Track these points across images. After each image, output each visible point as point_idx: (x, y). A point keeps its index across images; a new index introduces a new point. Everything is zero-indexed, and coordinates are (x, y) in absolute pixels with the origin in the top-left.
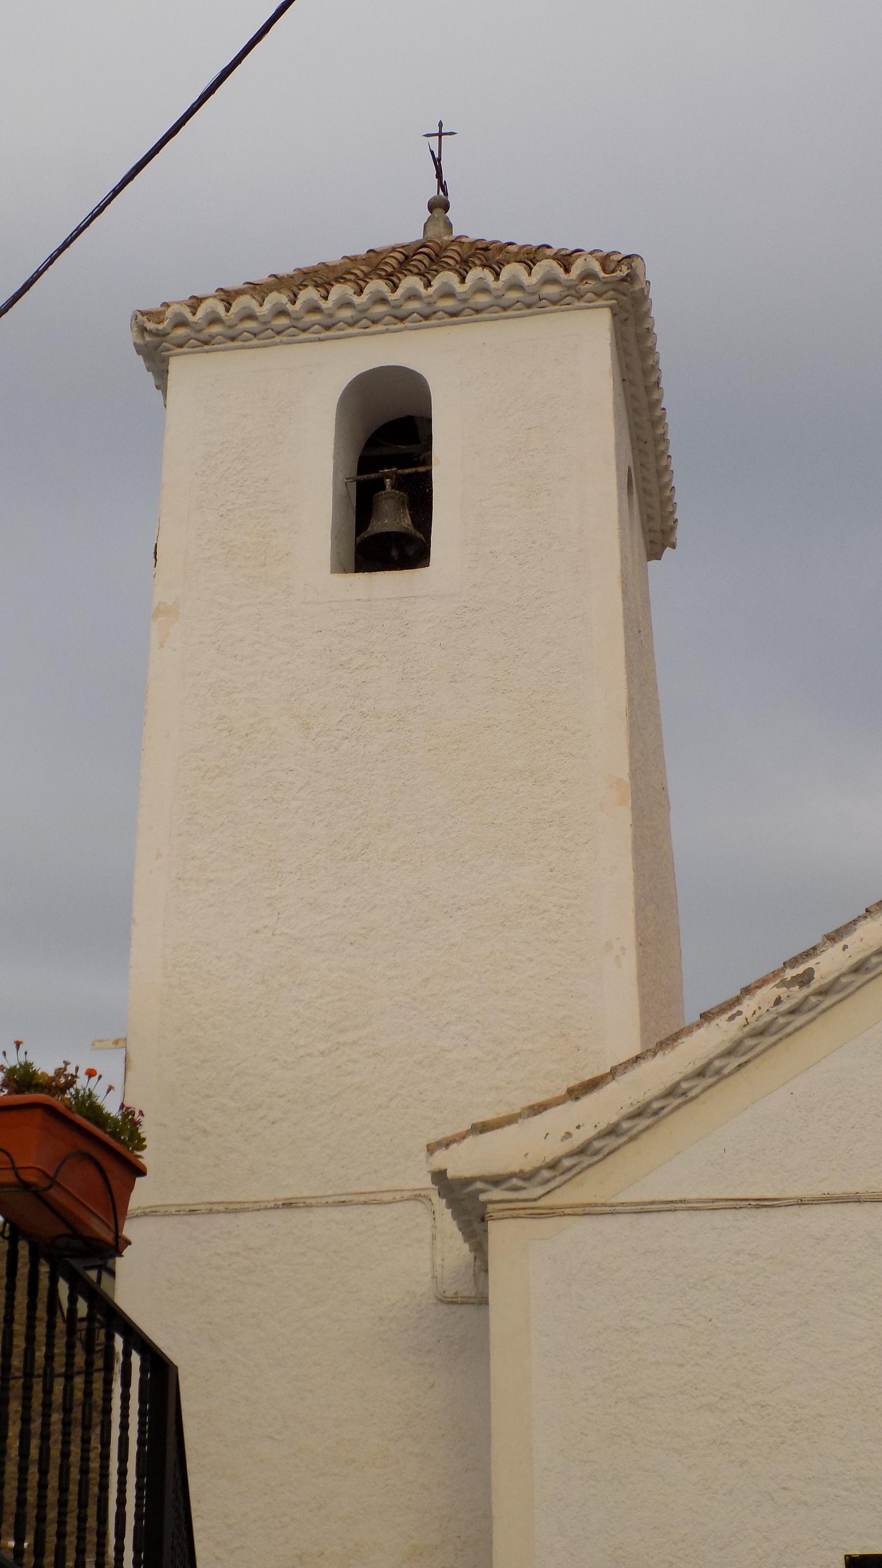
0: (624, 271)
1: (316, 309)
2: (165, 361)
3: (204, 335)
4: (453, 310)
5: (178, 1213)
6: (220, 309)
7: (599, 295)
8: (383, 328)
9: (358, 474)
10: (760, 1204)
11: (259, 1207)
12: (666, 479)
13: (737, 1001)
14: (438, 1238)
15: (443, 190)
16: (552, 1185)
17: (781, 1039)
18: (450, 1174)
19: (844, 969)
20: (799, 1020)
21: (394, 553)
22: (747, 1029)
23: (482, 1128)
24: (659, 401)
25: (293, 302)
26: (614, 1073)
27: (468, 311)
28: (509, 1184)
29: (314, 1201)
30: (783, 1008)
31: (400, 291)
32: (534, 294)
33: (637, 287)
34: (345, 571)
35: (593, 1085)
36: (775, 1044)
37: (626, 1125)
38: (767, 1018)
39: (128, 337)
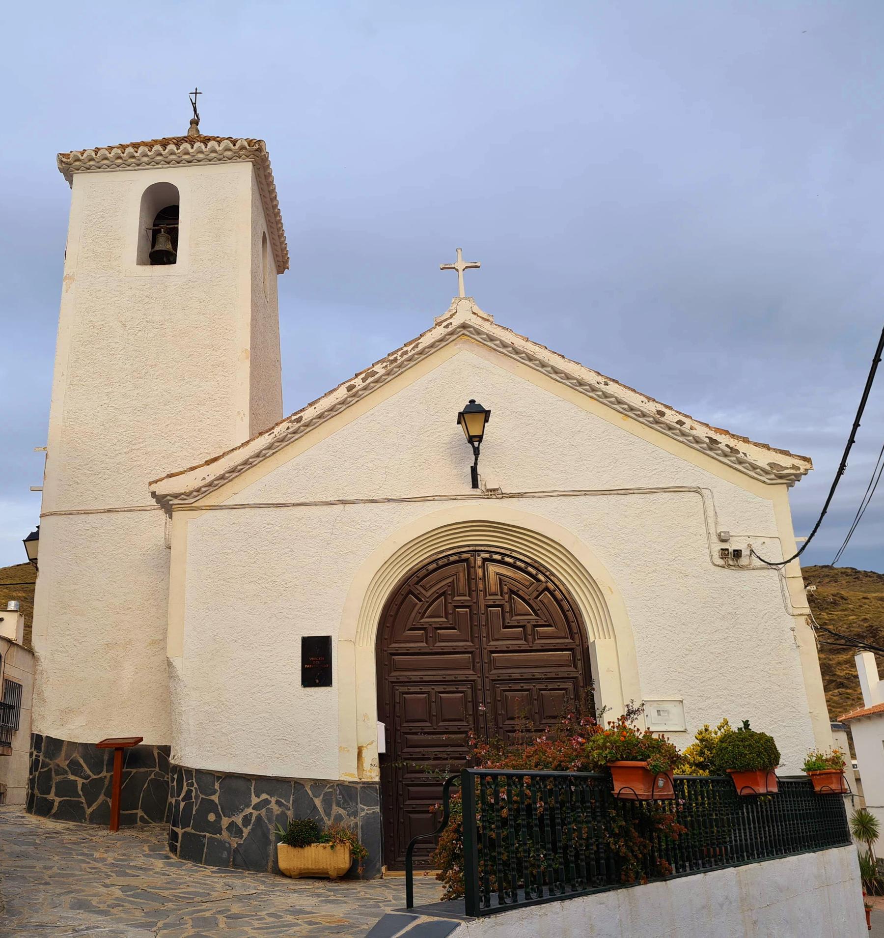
0: (257, 146)
1: (133, 157)
2: (72, 176)
3: (87, 165)
4: (189, 160)
5: (65, 514)
6: (93, 154)
7: (247, 157)
8: (161, 166)
13: (273, 428)
14: (168, 524)
15: (197, 116)
16: (198, 498)
18: (157, 493)
19: (314, 416)
21: (165, 259)
22: (275, 439)
23: (170, 476)
24: (277, 206)
25: (123, 153)
26: (223, 455)
27: (195, 161)
28: (180, 498)
29: (119, 510)
30: (290, 431)
31: (167, 150)
32: (221, 154)
33: (263, 154)
35: (215, 460)
36: (287, 445)
39: (55, 164)
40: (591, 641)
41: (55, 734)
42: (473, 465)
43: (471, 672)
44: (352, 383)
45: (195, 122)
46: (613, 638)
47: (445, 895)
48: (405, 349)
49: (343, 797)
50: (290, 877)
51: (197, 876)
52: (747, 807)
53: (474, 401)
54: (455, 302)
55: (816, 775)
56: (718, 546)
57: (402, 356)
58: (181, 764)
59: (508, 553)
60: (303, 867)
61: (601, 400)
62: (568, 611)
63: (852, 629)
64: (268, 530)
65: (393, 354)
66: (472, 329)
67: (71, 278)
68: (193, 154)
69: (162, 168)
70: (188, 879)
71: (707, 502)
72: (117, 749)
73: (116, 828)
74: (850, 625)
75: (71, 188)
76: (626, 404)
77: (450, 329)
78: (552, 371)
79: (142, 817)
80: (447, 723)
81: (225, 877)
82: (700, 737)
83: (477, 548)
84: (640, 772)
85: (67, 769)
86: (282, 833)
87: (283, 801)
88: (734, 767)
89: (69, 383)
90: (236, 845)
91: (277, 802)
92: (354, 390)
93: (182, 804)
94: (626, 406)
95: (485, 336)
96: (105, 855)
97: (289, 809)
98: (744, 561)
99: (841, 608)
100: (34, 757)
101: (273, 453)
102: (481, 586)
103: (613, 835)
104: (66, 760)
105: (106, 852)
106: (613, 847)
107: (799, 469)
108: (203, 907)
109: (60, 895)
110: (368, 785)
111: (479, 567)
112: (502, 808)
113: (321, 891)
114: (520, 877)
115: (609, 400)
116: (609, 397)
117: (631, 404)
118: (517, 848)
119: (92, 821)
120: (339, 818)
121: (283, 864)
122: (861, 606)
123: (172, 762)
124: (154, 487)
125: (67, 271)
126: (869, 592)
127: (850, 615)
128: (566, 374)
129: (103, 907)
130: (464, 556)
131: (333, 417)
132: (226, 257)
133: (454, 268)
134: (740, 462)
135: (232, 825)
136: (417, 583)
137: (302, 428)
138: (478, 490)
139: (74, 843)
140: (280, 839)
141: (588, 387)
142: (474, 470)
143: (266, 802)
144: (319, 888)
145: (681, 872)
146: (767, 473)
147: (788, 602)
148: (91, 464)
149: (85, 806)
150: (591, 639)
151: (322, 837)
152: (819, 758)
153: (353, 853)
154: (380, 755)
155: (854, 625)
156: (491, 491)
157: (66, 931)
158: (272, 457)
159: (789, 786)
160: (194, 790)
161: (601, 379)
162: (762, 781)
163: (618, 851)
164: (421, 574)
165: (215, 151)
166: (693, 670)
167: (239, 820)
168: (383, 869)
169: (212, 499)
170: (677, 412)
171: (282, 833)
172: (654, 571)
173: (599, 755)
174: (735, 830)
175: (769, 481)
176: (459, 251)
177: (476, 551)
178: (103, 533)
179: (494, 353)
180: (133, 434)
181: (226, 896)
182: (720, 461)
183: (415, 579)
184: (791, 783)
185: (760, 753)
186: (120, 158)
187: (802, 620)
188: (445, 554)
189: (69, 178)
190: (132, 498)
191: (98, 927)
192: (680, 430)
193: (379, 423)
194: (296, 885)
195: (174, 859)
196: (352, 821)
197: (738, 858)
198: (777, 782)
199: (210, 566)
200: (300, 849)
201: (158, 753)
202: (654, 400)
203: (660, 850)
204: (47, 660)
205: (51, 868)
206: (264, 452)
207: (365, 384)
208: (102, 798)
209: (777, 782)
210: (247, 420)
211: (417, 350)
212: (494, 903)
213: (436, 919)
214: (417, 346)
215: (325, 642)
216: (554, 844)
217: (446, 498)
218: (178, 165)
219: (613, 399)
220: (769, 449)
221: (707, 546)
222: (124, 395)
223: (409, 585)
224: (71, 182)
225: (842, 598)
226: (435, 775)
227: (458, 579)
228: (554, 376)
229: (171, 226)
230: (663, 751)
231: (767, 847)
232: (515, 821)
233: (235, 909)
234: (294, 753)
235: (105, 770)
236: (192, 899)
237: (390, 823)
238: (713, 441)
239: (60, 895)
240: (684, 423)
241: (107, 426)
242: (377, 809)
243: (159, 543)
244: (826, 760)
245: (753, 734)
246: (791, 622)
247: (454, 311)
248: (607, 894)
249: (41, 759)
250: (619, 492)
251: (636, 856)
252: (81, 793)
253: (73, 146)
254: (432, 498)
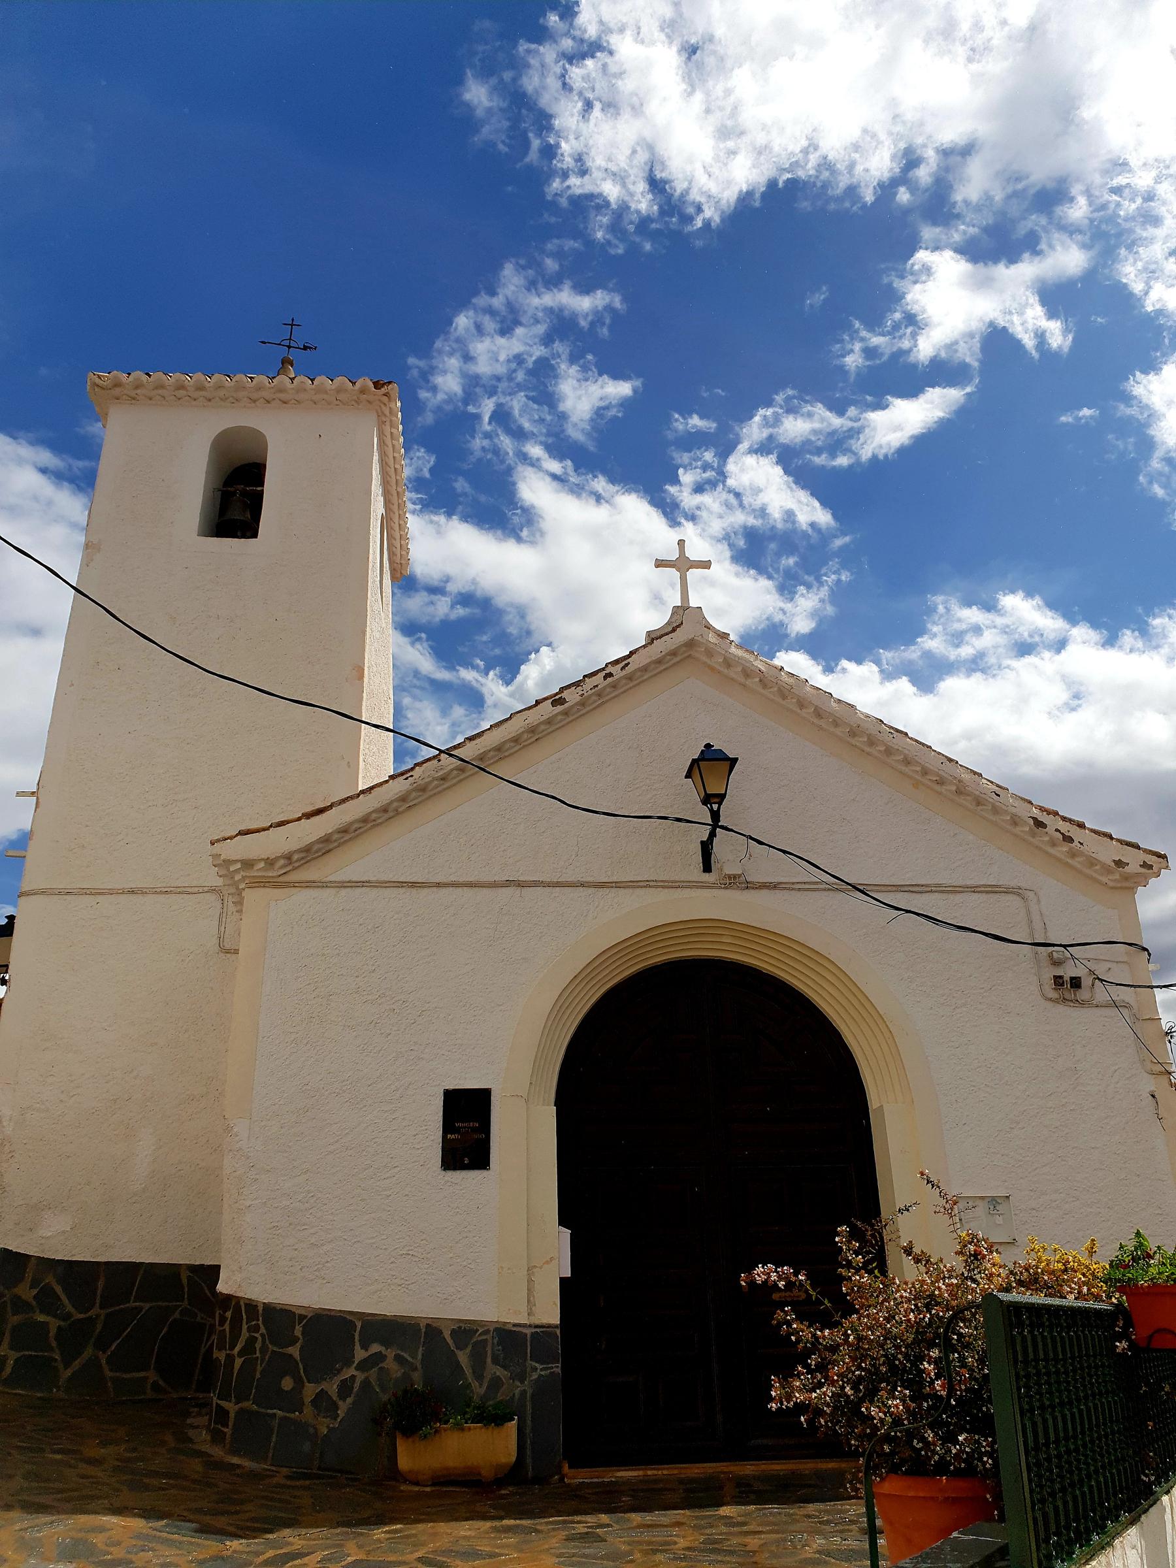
9: (223, 487)
10: (413, 885)
11: (111, 892)
17: (435, 794)
26: (331, 806)
85: (34, 1303)
87: (406, 1356)
91: (398, 1358)
93: (238, 1362)
143: (380, 1357)
160: (260, 1338)
215: (483, 1097)
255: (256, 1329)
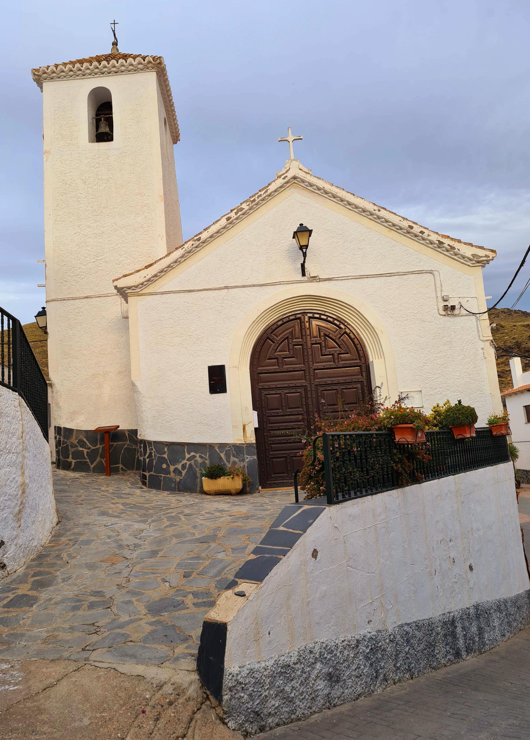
0: (158, 61)
1: (80, 70)
2: (42, 84)
4: (116, 71)
5: (61, 300)
6: (55, 69)
8: (98, 76)
12: (176, 122)
13: (184, 245)
18: (118, 287)
20: (198, 249)
23: (125, 276)
24: (172, 100)
25: (74, 68)
26: (155, 262)
27: (119, 72)
30: (194, 246)
31: (101, 65)
33: (162, 66)
34: (93, 142)
35: (151, 265)
36: (193, 255)
37: (158, 274)
38: (190, 249)
39: (31, 77)
40: (371, 361)
41: (68, 426)
42: (302, 262)
43: (304, 381)
44: (229, 215)
45: (115, 44)
46: (383, 359)
47: (306, 497)
48: (260, 193)
49: (236, 452)
50: (210, 495)
51: (160, 497)
52: (459, 445)
53: (302, 224)
54: (288, 162)
55: (494, 426)
56: (442, 304)
57: (258, 198)
58: (145, 439)
59: (323, 313)
60: (217, 489)
61: (376, 220)
62: (358, 344)
63: (506, 344)
64: (185, 306)
65: (253, 196)
66: (299, 180)
67: (48, 152)
68: (118, 67)
69: (99, 77)
70: (156, 498)
71: (436, 279)
72: (105, 432)
73: (109, 474)
74: (505, 342)
75: (42, 92)
76: (391, 222)
77: (286, 180)
78: (347, 204)
79: (122, 468)
80: (291, 410)
81: (175, 496)
82: (434, 410)
83: (306, 311)
84: (410, 430)
86: (204, 472)
87: (203, 456)
88: (454, 425)
89: (54, 220)
90: (179, 480)
91: (200, 457)
92: (231, 220)
93: (147, 460)
94: (390, 224)
95: (307, 184)
96: (108, 489)
97: (207, 460)
98: (456, 312)
99: (500, 332)
100: (58, 439)
101: (185, 260)
102: (308, 333)
103: (395, 462)
104: (76, 439)
105: (108, 487)
106: (395, 468)
107: (489, 257)
108: (169, 511)
109: (90, 509)
110: (249, 445)
111: (307, 322)
112: (337, 452)
113: (229, 500)
114: (346, 486)
115: (380, 220)
116: (381, 219)
117: (394, 222)
118: (344, 472)
119: (94, 472)
120: (234, 463)
121: (206, 488)
122: (512, 331)
123: (140, 438)
124: (116, 283)
125: (46, 147)
126: (517, 322)
127: (505, 336)
128: (355, 205)
129: (115, 514)
130: (298, 316)
131: (218, 237)
132: (144, 136)
133: (287, 140)
134: (456, 255)
135: (176, 470)
136: (272, 333)
137: (201, 244)
138: (305, 277)
139: (89, 483)
140: (203, 475)
141: (368, 213)
142: (303, 265)
143: (194, 457)
144: (227, 499)
145: (427, 479)
146: (471, 260)
147: (481, 333)
148: (73, 270)
149: (90, 464)
150: (371, 360)
151: (226, 473)
152: (496, 417)
153: (244, 480)
154: (255, 429)
155: (508, 342)
156: (313, 278)
157: (101, 526)
158: (184, 263)
159: (481, 432)
161: (376, 208)
162: (468, 431)
163: (398, 470)
164: (273, 328)
165: (132, 65)
166: (428, 374)
167: (179, 466)
168: (260, 488)
169: (151, 289)
170: (420, 226)
171: (204, 472)
172: (406, 320)
173: (388, 422)
174: (451, 457)
175: (472, 265)
176: (289, 129)
177: (304, 313)
178: (84, 311)
179: (312, 194)
180: (96, 250)
181: (179, 506)
182: (444, 255)
183: (271, 331)
184: (481, 431)
185: (468, 416)
186: (71, 71)
187: (488, 343)
188: (287, 315)
189: (40, 86)
190: (99, 289)
191: (117, 524)
192: (422, 237)
193: (246, 239)
194: (214, 498)
195: (145, 489)
196: (242, 464)
197: (454, 471)
198: (476, 431)
199: (152, 328)
200: (215, 480)
201: (128, 434)
202: (407, 219)
203: (417, 469)
204: (59, 385)
205: (81, 496)
206: (179, 259)
207: (237, 216)
208: (98, 459)
209: (476, 431)
210: (164, 239)
211: (267, 194)
212: (340, 498)
213: (313, 507)
214: (267, 191)
216: (362, 468)
217: (287, 283)
218: (109, 75)
219: (383, 220)
220: (472, 246)
221: (436, 304)
222: (89, 227)
223: (267, 334)
224: (41, 88)
225: (502, 326)
226: (298, 437)
227: (295, 330)
228: (348, 207)
229: (107, 116)
230: (422, 418)
231: (468, 464)
232: (343, 458)
233: (187, 511)
234: (208, 430)
235: (99, 444)
236: (162, 508)
237: (262, 464)
238: (441, 243)
239: (90, 509)
240: (424, 233)
241: (80, 246)
242: (255, 457)
243: (119, 315)
244: (499, 418)
245: (464, 407)
246: (482, 345)
247: (288, 168)
248: (392, 491)
249: (62, 439)
250: (387, 275)
251: (406, 472)
252: (86, 457)
253: (41, 63)
254: (279, 283)
255: (152, 449)
